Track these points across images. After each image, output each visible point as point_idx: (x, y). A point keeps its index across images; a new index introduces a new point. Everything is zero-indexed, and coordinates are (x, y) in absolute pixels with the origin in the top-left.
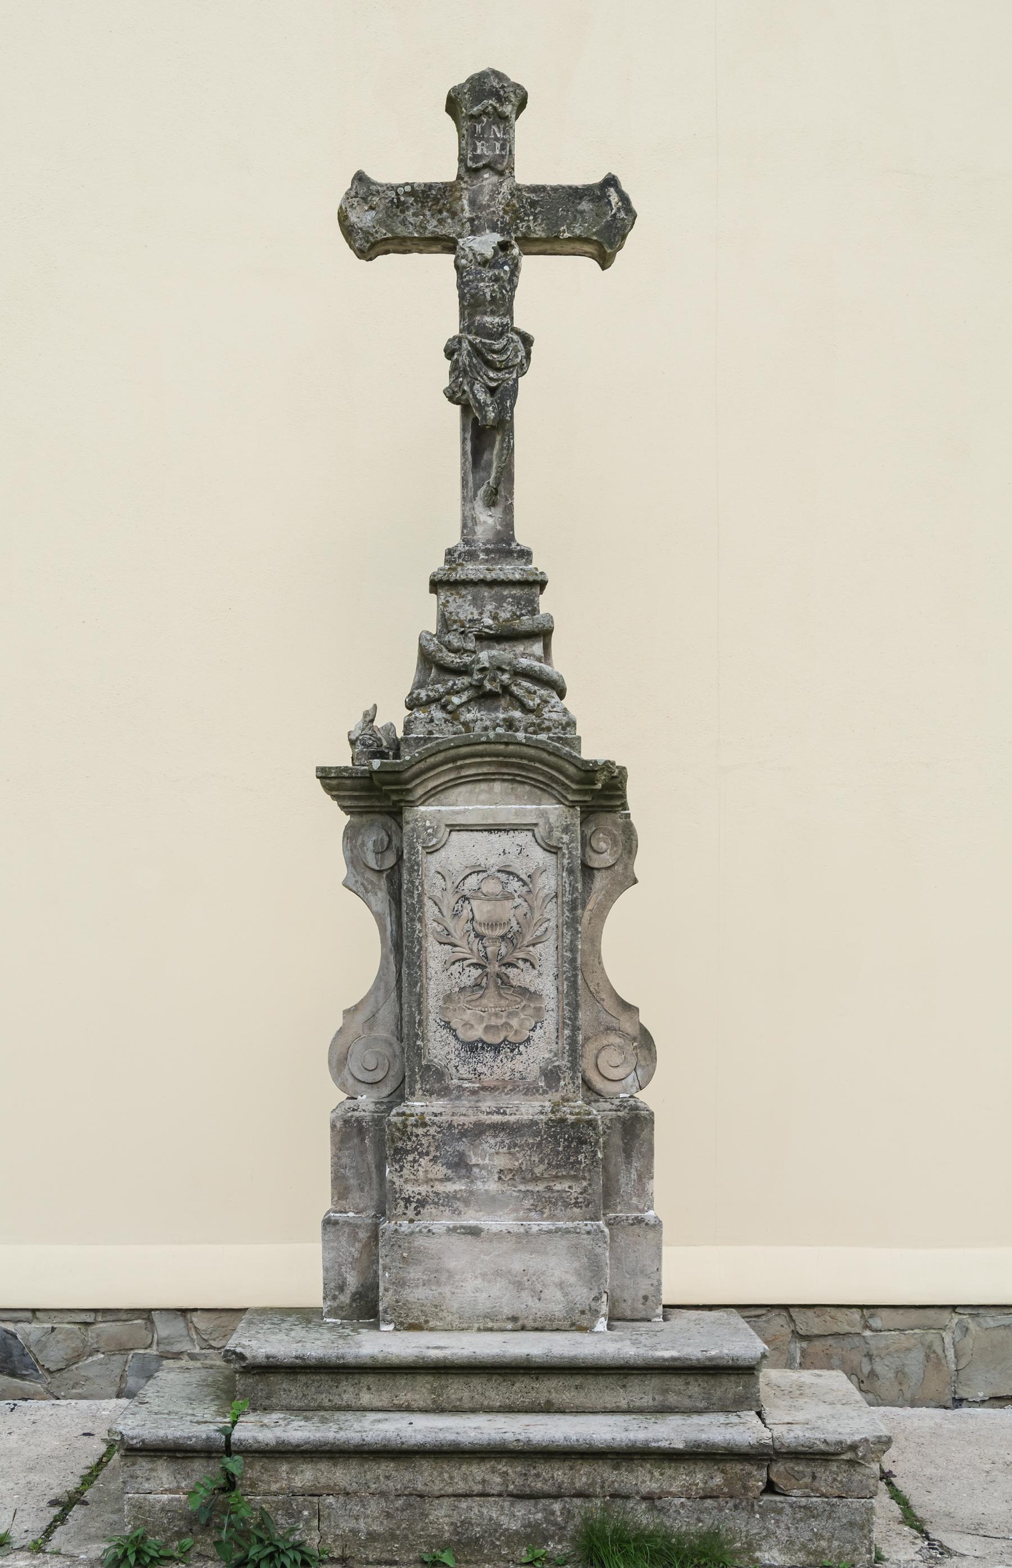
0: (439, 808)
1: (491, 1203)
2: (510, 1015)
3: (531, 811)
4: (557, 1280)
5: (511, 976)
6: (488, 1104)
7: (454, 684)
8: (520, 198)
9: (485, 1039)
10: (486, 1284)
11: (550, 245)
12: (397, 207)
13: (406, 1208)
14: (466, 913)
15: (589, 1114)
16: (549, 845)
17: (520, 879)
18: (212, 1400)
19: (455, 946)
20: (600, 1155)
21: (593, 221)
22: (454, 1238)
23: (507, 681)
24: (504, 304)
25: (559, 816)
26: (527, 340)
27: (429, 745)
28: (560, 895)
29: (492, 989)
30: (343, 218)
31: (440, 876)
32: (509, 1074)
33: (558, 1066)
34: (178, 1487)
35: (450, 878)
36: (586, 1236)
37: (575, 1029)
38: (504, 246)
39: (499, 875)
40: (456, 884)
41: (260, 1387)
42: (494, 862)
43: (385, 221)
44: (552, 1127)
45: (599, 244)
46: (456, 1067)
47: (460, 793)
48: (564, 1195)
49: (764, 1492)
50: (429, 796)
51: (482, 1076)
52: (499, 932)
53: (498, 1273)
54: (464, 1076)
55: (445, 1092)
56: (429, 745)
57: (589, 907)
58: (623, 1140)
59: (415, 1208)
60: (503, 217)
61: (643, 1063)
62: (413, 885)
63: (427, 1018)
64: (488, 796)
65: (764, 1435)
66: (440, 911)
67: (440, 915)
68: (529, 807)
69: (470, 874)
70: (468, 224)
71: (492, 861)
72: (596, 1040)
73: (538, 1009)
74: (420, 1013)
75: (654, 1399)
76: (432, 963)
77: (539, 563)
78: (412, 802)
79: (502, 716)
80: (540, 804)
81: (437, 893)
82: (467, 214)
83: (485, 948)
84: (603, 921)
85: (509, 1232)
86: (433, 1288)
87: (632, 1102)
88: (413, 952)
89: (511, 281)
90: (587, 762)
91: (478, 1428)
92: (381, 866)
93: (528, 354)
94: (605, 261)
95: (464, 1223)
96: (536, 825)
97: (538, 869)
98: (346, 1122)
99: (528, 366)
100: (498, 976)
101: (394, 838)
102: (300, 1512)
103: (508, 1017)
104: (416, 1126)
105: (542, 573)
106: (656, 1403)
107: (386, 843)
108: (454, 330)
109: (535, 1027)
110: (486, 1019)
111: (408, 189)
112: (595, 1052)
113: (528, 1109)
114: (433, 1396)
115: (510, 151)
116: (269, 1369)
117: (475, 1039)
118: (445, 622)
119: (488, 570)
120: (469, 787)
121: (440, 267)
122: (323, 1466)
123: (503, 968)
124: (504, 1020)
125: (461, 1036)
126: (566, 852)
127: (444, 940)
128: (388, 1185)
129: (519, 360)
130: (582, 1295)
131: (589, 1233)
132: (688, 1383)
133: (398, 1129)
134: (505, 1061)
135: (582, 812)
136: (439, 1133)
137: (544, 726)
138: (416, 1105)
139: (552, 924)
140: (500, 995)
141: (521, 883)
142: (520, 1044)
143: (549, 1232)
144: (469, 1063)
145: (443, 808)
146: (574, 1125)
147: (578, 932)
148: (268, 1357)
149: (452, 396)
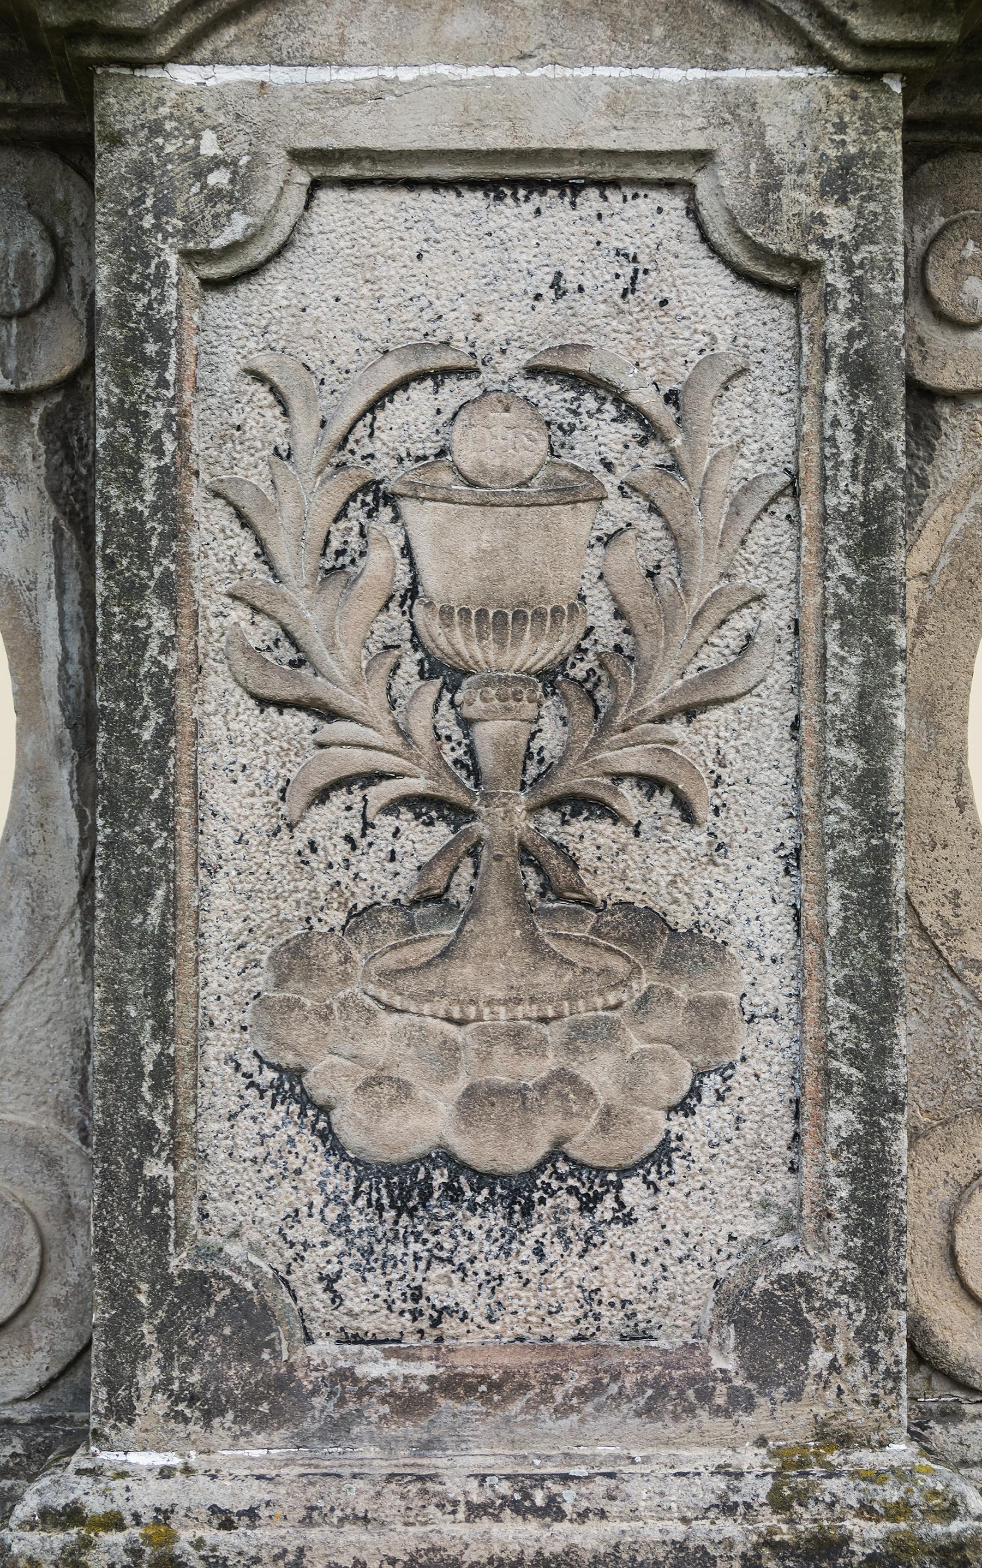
2: (583, 1036)
3: (683, 92)
5: (587, 855)
6: (477, 1458)
9: (463, 1148)
14: (380, 566)
15: (951, 1511)
17: (630, 411)
19: (329, 714)
25: (810, 117)
28: (810, 482)
29: (498, 920)
31: (262, 392)
32: (571, 1312)
33: (802, 1278)
35: (310, 399)
37: (879, 1103)
39: (536, 389)
42: (513, 328)
46: (329, 1282)
51: (450, 1326)
52: (533, 651)
54: (367, 1325)
55: (272, 1402)
62: (139, 431)
63: (196, 1055)
64: (484, 20)
66: (263, 554)
67: (262, 574)
68: (671, 74)
69: (403, 384)
71: (500, 325)
72: (948, 1144)
73: (709, 1012)
74: (163, 1029)
76: (223, 796)
78: (139, 37)
80: (720, 63)
81: (251, 471)
83: (466, 724)
88: (132, 742)
92: (20, 374)
96: (703, 158)
97: (710, 359)
100: (526, 854)
103: (570, 1047)
107: (40, 276)
109: (695, 1092)
110: (468, 1056)
112: (945, 1194)
117: (419, 1148)
123: (550, 819)
124: (551, 1063)
125: (351, 1136)
126: (841, 282)
127: (278, 688)
134: (554, 1251)
139: (776, 615)
140: (534, 943)
141: (631, 428)
142: (625, 1172)
144: (389, 1261)
147: (893, 655)
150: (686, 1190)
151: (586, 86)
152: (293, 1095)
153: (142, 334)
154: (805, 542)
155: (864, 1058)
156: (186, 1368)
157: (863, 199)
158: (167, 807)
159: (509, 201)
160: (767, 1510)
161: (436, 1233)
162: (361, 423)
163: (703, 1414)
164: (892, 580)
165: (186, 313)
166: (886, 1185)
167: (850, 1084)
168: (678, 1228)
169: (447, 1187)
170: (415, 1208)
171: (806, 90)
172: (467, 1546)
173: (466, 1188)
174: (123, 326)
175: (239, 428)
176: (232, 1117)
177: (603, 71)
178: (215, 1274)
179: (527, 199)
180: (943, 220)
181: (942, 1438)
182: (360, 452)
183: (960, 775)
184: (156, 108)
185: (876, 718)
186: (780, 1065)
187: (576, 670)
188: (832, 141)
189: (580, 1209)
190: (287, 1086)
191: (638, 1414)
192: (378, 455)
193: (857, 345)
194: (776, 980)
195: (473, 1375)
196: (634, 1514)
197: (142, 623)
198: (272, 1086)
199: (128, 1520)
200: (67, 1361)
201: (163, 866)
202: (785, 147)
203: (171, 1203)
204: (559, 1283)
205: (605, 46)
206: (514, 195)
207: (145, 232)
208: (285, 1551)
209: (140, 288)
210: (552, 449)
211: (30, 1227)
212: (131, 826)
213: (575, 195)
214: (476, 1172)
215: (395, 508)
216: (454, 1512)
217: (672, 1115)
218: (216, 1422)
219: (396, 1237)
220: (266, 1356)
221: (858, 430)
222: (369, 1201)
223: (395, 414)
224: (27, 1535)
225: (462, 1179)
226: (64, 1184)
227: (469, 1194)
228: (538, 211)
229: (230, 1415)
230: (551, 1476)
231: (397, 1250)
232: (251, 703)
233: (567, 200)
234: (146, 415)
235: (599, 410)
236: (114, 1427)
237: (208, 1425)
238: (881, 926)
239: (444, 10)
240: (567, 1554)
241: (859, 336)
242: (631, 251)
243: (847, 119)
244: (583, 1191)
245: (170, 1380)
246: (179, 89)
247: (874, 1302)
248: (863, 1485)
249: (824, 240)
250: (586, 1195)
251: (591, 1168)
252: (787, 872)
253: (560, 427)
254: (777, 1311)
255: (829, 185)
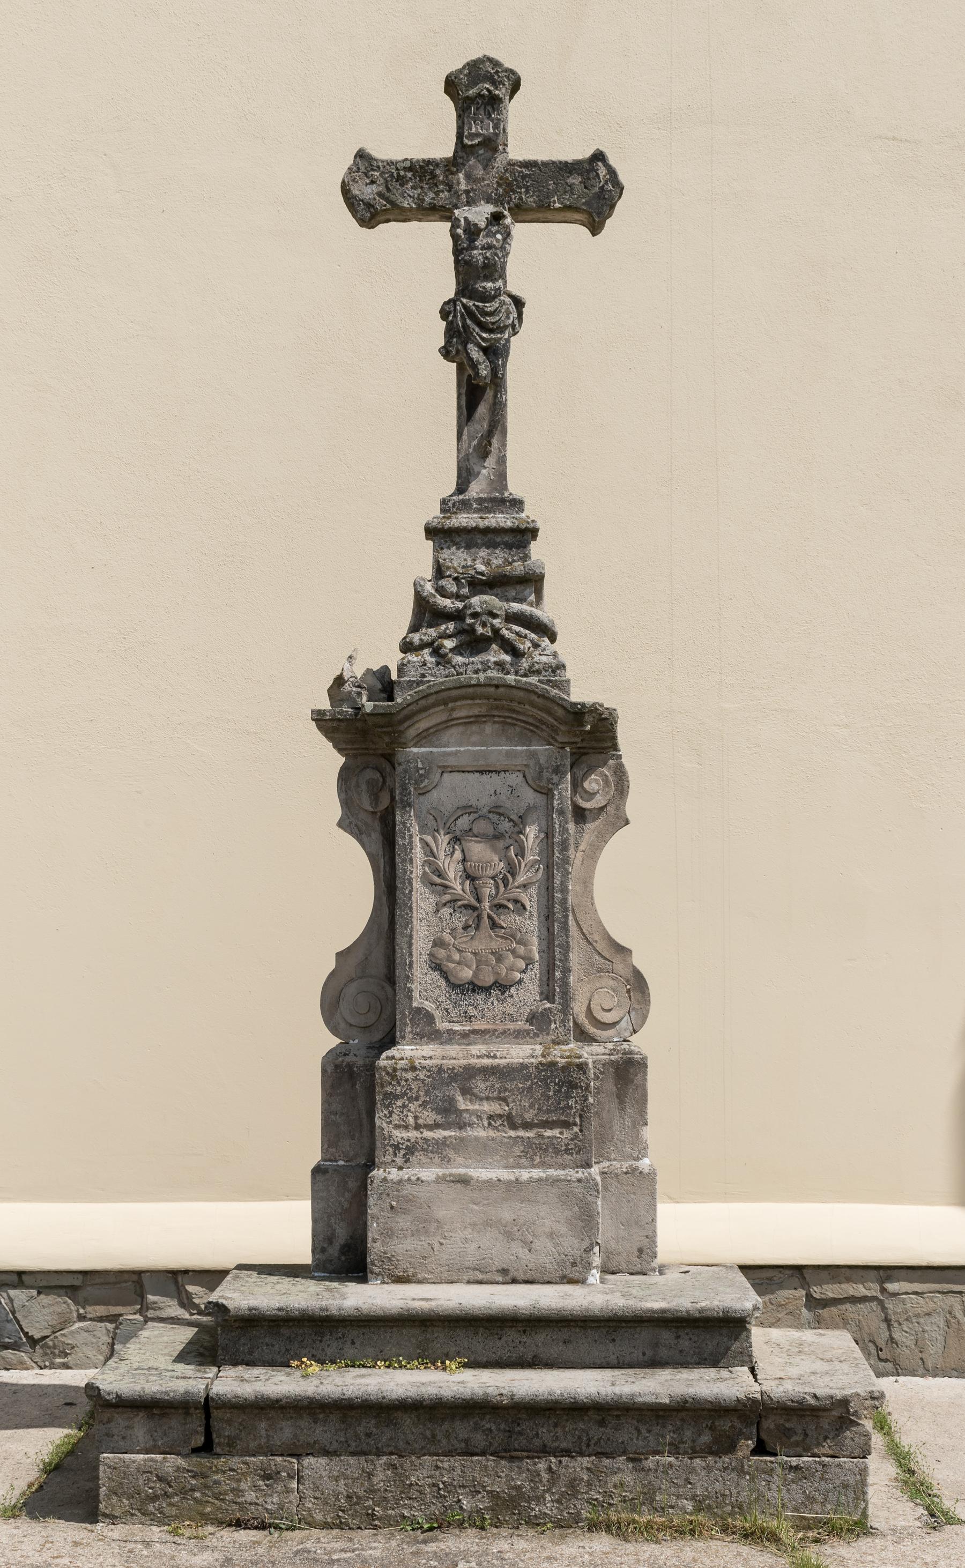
0: (431, 749)
1: (483, 1151)
3: (522, 751)
4: (547, 1230)
7: (447, 628)
8: (513, 173)
10: (475, 1234)
11: (540, 211)
12: (397, 181)
13: (395, 1155)
15: (580, 1057)
16: (539, 786)
17: (511, 820)
18: (195, 1357)
20: (591, 1100)
21: (585, 192)
22: (443, 1187)
23: (498, 625)
24: (493, 270)
26: (519, 303)
27: (421, 688)
30: (346, 191)
34: (155, 1446)
36: (576, 1184)
38: (496, 218)
39: (491, 816)
40: (447, 826)
41: (242, 1341)
42: (485, 802)
43: (381, 193)
44: (542, 1071)
45: (590, 214)
47: (451, 735)
48: (555, 1141)
49: (755, 1452)
50: (423, 738)
53: (488, 1224)
56: (421, 688)
57: (581, 848)
58: (616, 1085)
59: (404, 1155)
60: (497, 190)
61: (637, 1006)
65: (753, 1389)
68: (519, 748)
70: (464, 196)
74: (411, 955)
75: (644, 1354)
77: (530, 513)
79: (493, 659)
82: (463, 187)
84: (596, 862)
85: (499, 1180)
86: (423, 1238)
87: (625, 1046)
88: (404, 893)
89: (503, 248)
90: (576, 704)
91: (463, 1382)
93: (520, 315)
94: (595, 228)
95: (454, 1171)
98: (337, 1066)
99: (520, 326)
101: (388, 779)
102: (279, 1473)
104: (405, 1070)
105: (533, 521)
106: (646, 1358)
108: (450, 294)
111: (408, 164)
113: (520, 1053)
114: (419, 1351)
115: (504, 130)
116: (253, 1322)
118: (439, 572)
119: (482, 518)
120: (461, 729)
121: (437, 234)
122: (305, 1423)
128: (378, 1130)
129: (510, 321)
130: (572, 1245)
131: (579, 1181)
132: (678, 1337)
133: (388, 1073)
134: (496, 1003)
135: (572, 754)
136: (428, 1077)
137: (534, 669)
138: (406, 1051)
143: (540, 1180)
144: (460, 1006)
145: (435, 750)
146: (565, 1068)
148: (250, 1309)
149: (446, 353)
151: (501, 751)
223: (459, 822)
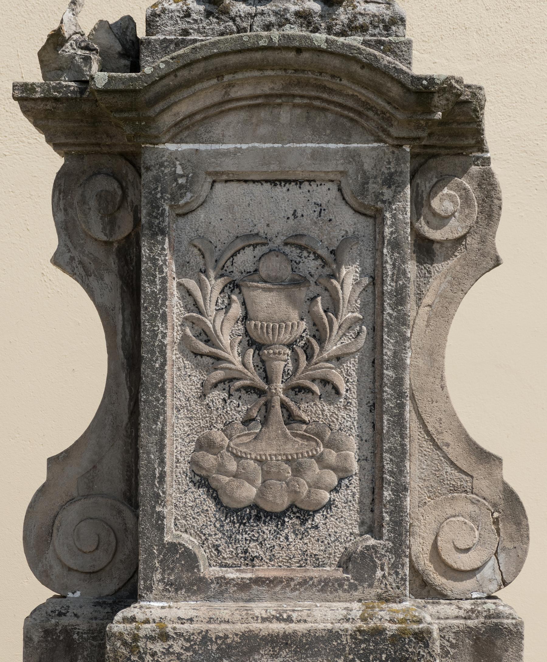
3: (336, 151)
17: (318, 257)
39: (287, 249)
42: (280, 228)
54: (229, 562)
68: (332, 146)
71: (276, 228)
88: (153, 367)
112: (434, 526)
134: (292, 537)
144: (237, 541)
147: (406, 339)
150: (336, 518)
151: (304, 150)
152: (205, 485)
153: (157, 233)
154: (377, 301)
155: (394, 474)
156: (169, 574)
157: (396, 187)
158: (164, 389)
159: (278, 186)
160: (359, 621)
161: (252, 531)
162: (229, 261)
163: (340, 592)
164: (405, 314)
165: (171, 225)
166: (402, 516)
167: (390, 482)
168: (333, 530)
169: (256, 516)
170: (245, 523)
171: (377, 151)
172: (261, 630)
173: (263, 517)
174: (290, 645)
175: (188, 263)
176: (186, 491)
177: (309, 145)
178: (179, 544)
179: (285, 186)
180: (436, 179)
181: (431, 610)
182: (228, 270)
183: (442, 376)
184: (162, 158)
185: (399, 360)
186: (368, 476)
187: (300, 343)
188: (386, 167)
189: (301, 524)
190: (203, 482)
191: (319, 591)
192: (234, 271)
193: (394, 236)
194: (367, 448)
195: (264, 578)
196: (315, 621)
197: (156, 328)
198: (198, 482)
199: (151, 621)
200: (125, 582)
201: (162, 409)
202: (370, 170)
203: (165, 520)
204: (293, 549)
205: (310, 137)
206: (280, 184)
207: (158, 199)
208: (202, 631)
209: (156, 217)
210: (292, 269)
211: (112, 534)
212: (152, 395)
213: (300, 184)
214: (266, 511)
215: (240, 289)
216: (257, 620)
217: (332, 493)
218: (179, 593)
219: (239, 532)
220: (196, 571)
221: (394, 264)
222: (230, 520)
223: (239, 259)
224: (119, 625)
225: (261, 514)
226: (124, 519)
227: (263, 518)
228: (288, 190)
229: (184, 590)
230: (289, 610)
231: (239, 537)
232: (192, 354)
233: (298, 186)
234: (158, 259)
235: (308, 256)
236: (146, 594)
237: (176, 593)
238: (401, 430)
239: (257, 125)
240: (293, 633)
241: (395, 233)
242: (320, 203)
243: (391, 160)
244: (302, 518)
245: (164, 578)
246: (169, 152)
247: (398, 555)
248: (391, 613)
249: (383, 201)
250: (303, 519)
251: (304, 510)
252: (371, 411)
253: (295, 262)
254: (365, 558)
255: (385, 182)
